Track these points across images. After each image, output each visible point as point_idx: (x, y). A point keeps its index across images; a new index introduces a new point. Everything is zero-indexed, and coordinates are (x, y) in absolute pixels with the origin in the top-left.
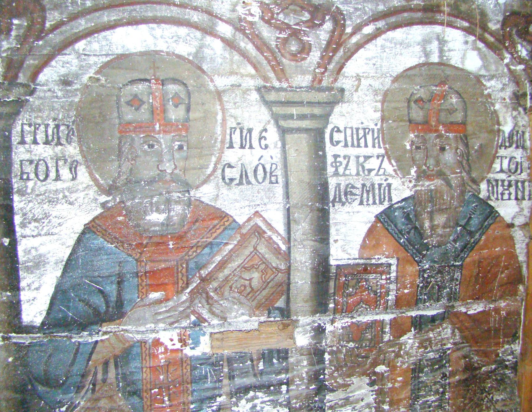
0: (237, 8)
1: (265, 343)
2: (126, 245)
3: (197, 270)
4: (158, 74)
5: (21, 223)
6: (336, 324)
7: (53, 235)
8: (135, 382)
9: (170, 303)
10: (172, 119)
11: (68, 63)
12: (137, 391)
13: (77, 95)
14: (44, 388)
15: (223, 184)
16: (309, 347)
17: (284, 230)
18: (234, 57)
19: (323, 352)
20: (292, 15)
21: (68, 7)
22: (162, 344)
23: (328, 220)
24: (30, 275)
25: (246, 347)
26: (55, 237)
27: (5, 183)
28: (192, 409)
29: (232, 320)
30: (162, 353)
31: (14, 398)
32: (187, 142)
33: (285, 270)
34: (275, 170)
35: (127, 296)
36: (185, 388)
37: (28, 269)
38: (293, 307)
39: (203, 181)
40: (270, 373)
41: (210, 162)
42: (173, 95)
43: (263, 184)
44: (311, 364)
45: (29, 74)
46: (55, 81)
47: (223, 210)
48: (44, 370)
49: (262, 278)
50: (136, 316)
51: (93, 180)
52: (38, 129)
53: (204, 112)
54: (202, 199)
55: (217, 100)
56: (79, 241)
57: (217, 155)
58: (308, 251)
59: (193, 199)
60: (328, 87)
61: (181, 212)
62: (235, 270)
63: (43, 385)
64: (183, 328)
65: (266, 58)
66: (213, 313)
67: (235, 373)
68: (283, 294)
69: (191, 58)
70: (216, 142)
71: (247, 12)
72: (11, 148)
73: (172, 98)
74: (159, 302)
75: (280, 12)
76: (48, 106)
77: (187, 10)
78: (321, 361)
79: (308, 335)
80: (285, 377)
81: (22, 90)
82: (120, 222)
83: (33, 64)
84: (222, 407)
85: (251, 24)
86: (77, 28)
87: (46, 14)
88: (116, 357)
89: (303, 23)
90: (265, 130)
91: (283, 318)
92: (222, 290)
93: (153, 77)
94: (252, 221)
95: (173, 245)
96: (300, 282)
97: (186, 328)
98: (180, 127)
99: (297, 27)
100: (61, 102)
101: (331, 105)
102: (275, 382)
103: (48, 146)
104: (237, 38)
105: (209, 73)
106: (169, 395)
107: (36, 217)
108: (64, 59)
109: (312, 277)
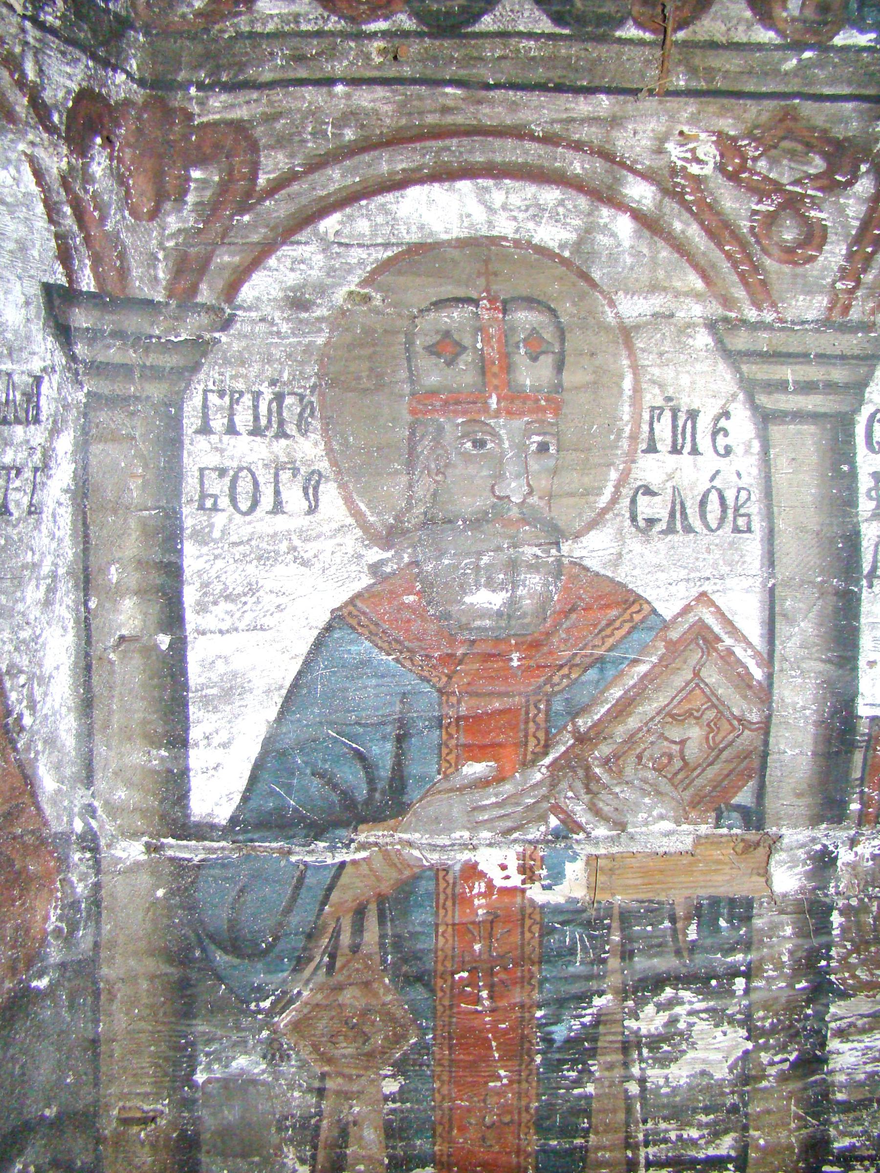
0: (666, 145)
1: (702, 884)
2: (418, 658)
3: (569, 718)
4: (494, 287)
5: (198, 603)
6: (859, 849)
7: (265, 630)
8: (419, 955)
9: (507, 787)
10: (525, 386)
11: (302, 262)
12: (424, 973)
13: (321, 330)
14: (226, 958)
15: (633, 529)
16: (800, 896)
17: (762, 636)
18: (658, 252)
19: (830, 909)
20: (785, 162)
21: (305, 141)
22: (482, 875)
23: (857, 616)
24: (210, 715)
25: (663, 890)
26: (267, 635)
27: (167, 516)
28: (538, 1019)
29: (638, 830)
30: (480, 894)
31: (166, 974)
32: (557, 435)
33: (757, 723)
34: (745, 503)
35: (414, 769)
36: (526, 974)
37: (207, 702)
38: (771, 804)
39: (589, 523)
40: (713, 949)
41: (607, 481)
42: (527, 333)
43: (719, 532)
44: (801, 933)
45: (220, 284)
46: (275, 299)
47: (630, 586)
48: (229, 921)
49: (707, 738)
50: (431, 811)
51: (352, 515)
52: (237, 401)
53: (595, 372)
54: (587, 563)
55: (622, 346)
56: (318, 644)
57: (621, 467)
58: (811, 683)
59: (566, 561)
60: (862, 322)
61: (539, 588)
62: (652, 719)
63: (225, 951)
64: (530, 842)
65: (729, 256)
66: (596, 811)
67: (636, 945)
68: (750, 777)
69: (567, 254)
70: (619, 437)
71: (689, 155)
72: (181, 443)
73: (524, 340)
74: (483, 783)
75: (760, 155)
76: (259, 353)
77: (560, 150)
78: (824, 927)
79: (800, 869)
80: (744, 960)
81: (204, 319)
82: (409, 606)
83: (229, 263)
84: (603, 1018)
85: (698, 180)
86: (324, 187)
87: (259, 157)
88: (381, 899)
89: (811, 180)
90: (726, 414)
91: (748, 830)
92: (620, 762)
93: (484, 294)
94: (692, 614)
95: (519, 660)
96: (790, 753)
97: (537, 842)
98: (543, 403)
99: (798, 189)
100: (286, 346)
101: (869, 363)
102: (720, 970)
103: (258, 439)
104: (667, 210)
105: (605, 288)
106: (491, 987)
107: (230, 590)
108: (294, 254)
109: (816, 743)
